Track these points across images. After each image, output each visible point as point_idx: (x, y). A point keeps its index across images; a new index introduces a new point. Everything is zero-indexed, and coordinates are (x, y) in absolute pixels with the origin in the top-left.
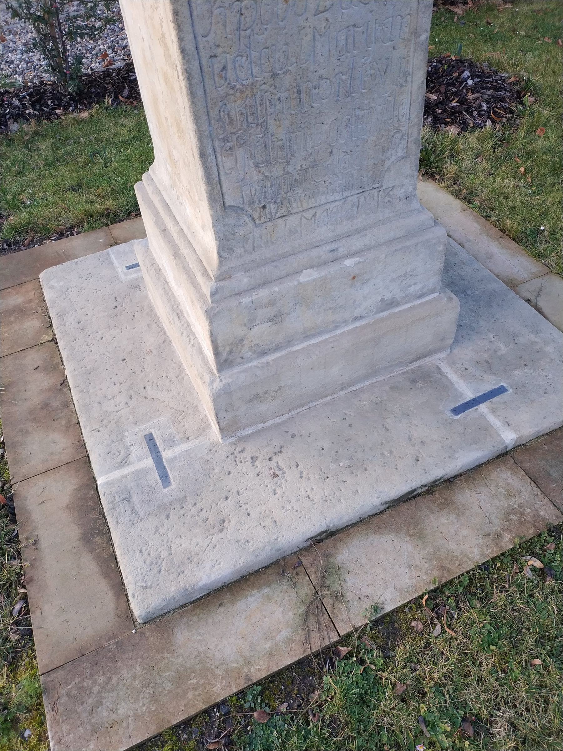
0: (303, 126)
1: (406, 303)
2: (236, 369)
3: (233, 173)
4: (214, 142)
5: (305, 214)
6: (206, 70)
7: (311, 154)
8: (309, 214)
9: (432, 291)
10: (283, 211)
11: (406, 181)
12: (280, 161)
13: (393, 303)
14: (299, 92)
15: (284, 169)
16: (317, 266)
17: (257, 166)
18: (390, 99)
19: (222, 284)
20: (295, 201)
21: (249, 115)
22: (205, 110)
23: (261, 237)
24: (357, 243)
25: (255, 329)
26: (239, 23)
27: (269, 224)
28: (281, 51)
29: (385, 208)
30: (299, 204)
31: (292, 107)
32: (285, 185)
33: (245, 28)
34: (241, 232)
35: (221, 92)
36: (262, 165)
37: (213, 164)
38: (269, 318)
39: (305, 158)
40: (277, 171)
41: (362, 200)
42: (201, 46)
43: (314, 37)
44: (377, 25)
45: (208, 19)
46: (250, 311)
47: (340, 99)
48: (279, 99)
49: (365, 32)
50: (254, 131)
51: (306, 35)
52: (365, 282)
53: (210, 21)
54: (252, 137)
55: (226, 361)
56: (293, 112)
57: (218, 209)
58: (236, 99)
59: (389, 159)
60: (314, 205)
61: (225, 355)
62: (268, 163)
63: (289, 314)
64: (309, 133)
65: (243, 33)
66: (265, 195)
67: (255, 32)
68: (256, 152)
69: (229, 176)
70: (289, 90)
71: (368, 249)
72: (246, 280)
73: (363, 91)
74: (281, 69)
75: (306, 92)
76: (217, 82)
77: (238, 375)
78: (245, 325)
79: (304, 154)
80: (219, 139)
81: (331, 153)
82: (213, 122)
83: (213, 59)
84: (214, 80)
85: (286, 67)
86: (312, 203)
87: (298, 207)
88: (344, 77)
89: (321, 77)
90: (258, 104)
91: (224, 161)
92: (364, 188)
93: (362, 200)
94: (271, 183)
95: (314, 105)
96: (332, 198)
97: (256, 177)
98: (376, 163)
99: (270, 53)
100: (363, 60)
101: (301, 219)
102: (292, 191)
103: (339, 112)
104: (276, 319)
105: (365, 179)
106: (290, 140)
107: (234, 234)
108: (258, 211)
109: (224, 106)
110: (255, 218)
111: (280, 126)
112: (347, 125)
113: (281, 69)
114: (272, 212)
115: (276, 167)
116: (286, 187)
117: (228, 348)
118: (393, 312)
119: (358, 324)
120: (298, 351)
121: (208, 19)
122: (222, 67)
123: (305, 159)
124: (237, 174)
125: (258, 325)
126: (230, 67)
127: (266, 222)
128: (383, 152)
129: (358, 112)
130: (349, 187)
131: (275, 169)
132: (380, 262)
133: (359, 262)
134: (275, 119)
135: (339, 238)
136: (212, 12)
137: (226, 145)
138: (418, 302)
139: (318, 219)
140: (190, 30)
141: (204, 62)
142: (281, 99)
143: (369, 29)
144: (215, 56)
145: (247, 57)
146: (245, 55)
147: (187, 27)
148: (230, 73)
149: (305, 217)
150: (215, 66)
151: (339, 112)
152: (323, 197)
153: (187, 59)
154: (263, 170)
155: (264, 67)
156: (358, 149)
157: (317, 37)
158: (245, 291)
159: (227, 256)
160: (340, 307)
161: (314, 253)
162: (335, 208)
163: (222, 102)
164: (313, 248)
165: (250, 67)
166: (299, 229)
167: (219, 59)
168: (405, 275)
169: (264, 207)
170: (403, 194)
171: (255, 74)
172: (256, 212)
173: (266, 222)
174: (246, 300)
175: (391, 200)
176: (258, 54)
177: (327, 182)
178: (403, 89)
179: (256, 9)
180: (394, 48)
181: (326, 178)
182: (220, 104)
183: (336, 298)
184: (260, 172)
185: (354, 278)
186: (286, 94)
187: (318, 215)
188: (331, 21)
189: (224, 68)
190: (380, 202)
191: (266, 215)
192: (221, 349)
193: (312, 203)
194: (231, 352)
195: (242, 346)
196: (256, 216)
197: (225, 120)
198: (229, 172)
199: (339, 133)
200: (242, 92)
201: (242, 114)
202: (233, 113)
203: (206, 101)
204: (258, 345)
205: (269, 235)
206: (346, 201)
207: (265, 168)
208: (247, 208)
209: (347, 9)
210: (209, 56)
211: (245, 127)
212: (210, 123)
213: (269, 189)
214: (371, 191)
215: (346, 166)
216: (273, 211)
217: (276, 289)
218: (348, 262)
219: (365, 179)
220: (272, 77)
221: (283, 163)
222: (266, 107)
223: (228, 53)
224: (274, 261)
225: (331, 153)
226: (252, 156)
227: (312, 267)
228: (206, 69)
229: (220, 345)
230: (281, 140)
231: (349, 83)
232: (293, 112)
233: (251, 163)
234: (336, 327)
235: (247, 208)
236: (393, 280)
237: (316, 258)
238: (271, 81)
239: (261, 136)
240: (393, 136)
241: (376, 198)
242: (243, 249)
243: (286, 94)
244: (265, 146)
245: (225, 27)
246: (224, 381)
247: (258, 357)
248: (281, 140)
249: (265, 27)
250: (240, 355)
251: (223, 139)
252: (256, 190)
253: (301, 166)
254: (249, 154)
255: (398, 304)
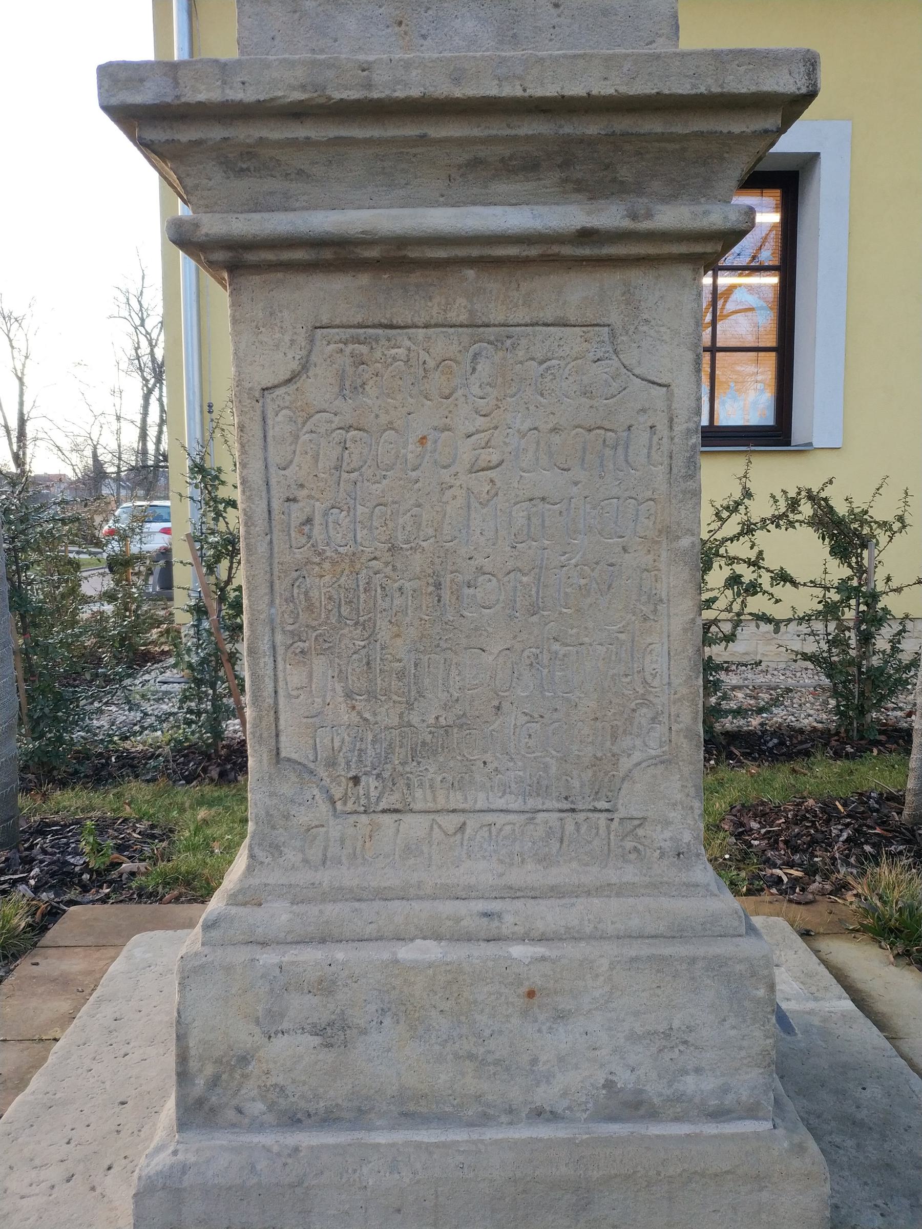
0: (443, 645)
1: (677, 1119)
2: (222, 1139)
3: (302, 697)
4: (276, 635)
5: (439, 818)
6: (277, 517)
7: (457, 700)
8: (450, 822)
9: (752, 1112)
10: (391, 800)
11: (674, 815)
12: (395, 698)
13: (635, 1107)
14: (438, 586)
15: (401, 715)
16: (450, 939)
17: (349, 695)
18: (622, 636)
19: (234, 910)
20: (421, 785)
21: (343, 602)
22: (268, 576)
23: (342, 841)
24: (549, 915)
25: (280, 1042)
26: (340, 459)
27: (364, 819)
28: (409, 514)
29: (626, 861)
30: (429, 797)
31: (424, 608)
32: (401, 747)
33: (348, 469)
34: (303, 817)
35: (298, 556)
36: (358, 697)
37: (268, 672)
38: (314, 1025)
39: (445, 704)
40: (388, 715)
41: (570, 827)
42: (273, 482)
43: (469, 503)
44: (588, 506)
45: (291, 445)
46: (272, 990)
47: (517, 614)
48: (400, 589)
49: (565, 513)
50: (350, 632)
51: (454, 498)
52: (561, 1016)
53: (293, 447)
54: (344, 642)
55: (200, 1102)
56: (427, 618)
57: (265, 757)
58: (324, 574)
59: (629, 755)
60: (462, 806)
61: (200, 1084)
62: (372, 695)
63: (364, 1032)
64: (455, 661)
65: (345, 476)
66: (360, 756)
67: (365, 477)
68: (350, 670)
69: (293, 700)
70: (419, 579)
71: (573, 936)
72: (285, 917)
73: (565, 610)
74: (407, 542)
75: (451, 588)
76: (293, 539)
77: (218, 1154)
78: (257, 1022)
79: (444, 696)
80: (284, 632)
81: (498, 708)
82: (277, 601)
83: (292, 503)
84: (290, 535)
85: (416, 541)
86: (456, 800)
87: (426, 801)
88: (525, 579)
89: (480, 570)
90: (361, 588)
91: (288, 671)
92: (572, 802)
93: (570, 827)
94: (375, 736)
95: (465, 613)
96: (500, 803)
97: (346, 717)
98: (599, 755)
99: (389, 512)
100: (563, 558)
101: (432, 828)
102: (415, 764)
103: (515, 637)
104: (332, 1033)
105: (576, 783)
106: (416, 665)
107: (287, 817)
108: (344, 784)
109: (301, 580)
110: (336, 798)
111: (398, 636)
112: (531, 665)
113: (407, 542)
114: (372, 794)
115: (386, 707)
116: (403, 750)
117: (209, 1070)
118: (643, 1131)
119: (544, 1132)
120: (378, 1146)
121: (291, 445)
122: (305, 518)
123: (445, 707)
124: (310, 701)
125: (288, 1032)
126: (318, 519)
127: (356, 812)
128: (614, 737)
129: (556, 646)
130: (539, 789)
131: (383, 709)
132: (597, 976)
133: (543, 959)
134: (390, 622)
135: (513, 893)
136: (297, 437)
137: (295, 645)
138: (711, 1129)
139: (470, 839)
140: (260, 454)
141: (276, 505)
142: (404, 590)
143: (572, 511)
144: (294, 500)
145: (348, 512)
146: (345, 507)
147: (256, 450)
148: (317, 531)
149: (440, 827)
150: (293, 516)
151: (515, 637)
152: (481, 796)
153: (248, 494)
154: (359, 706)
155: (376, 532)
156: (556, 716)
157: (474, 504)
158: (278, 943)
159: (267, 861)
160: (497, 1063)
161: (448, 908)
162: (508, 828)
163: (298, 573)
164: (449, 898)
165: (352, 527)
166: (425, 849)
167: (301, 504)
168: (667, 1035)
169: (356, 780)
170: (668, 843)
171: (359, 540)
172: (339, 784)
173: (356, 812)
174: (269, 958)
175: (640, 847)
176: (367, 510)
177: (491, 767)
178: (648, 624)
179: (371, 445)
180: (625, 549)
181: (488, 757)
182: (295, 574)
183: (487, 1033)
184: (354, 708)
185: (531, 994)
186: (415, 584)
187: (468, 831)
188: (498, 484)
189: (309, 521)
190: (612, 844)
191: (358, 798)
192: (193, 1065)
193: (456, 800)
194: (215, 1082)
195: (245, 1076)
196: (337, 792)
197: (300, 602)
198: (295, 693)
199: (515, 675)
200: (334, 563)
201: (330, 598)
202: (314, 594)
203: (271, 564)
204: (282, 1089)
205: (359, 844)
206: (533, 818)
207: (363, 703)
208: (322, 773)
209: (529, 472)
210: (284, 497)
211: (334, 621)
212: (272, 603)
213: (369, 747)
214: (590, 815)
215: (531, 743)
216: (374, 794)
217: (340, 956)
218: (518, 951)
219: (576, 783)
220: (389, 550)
221: (399, 702)
222: (375, 596)
223: (318, 500)
224: (359, 900)
225: (498, 708)
226: (342, 676)
227: (438, 938)
228: (276, 515)
229: (193, 1052)
230: (400, 661)
231: (534, 590)
232: (427, 618)
233: (339, 688)
234: (485, 1119)
235: (322, 773)
236: (634, 1038)
237: (448, 918)
238: (387, 557)
239: (362, 643)
240: (634, 710)
241: (602, 831)
242: (300, 856)
243: (415, 584)
244: (368, 663)
245: (317, 462)
246: (180, 1157)
247: (278, 1125)
248: (400, 661)
249: (384, 473)
250: (234, 1102)
251: (292, 632)
252: (343, 742)
253: (437, 718)
254: (337, 670)
255: (654, 1115)
